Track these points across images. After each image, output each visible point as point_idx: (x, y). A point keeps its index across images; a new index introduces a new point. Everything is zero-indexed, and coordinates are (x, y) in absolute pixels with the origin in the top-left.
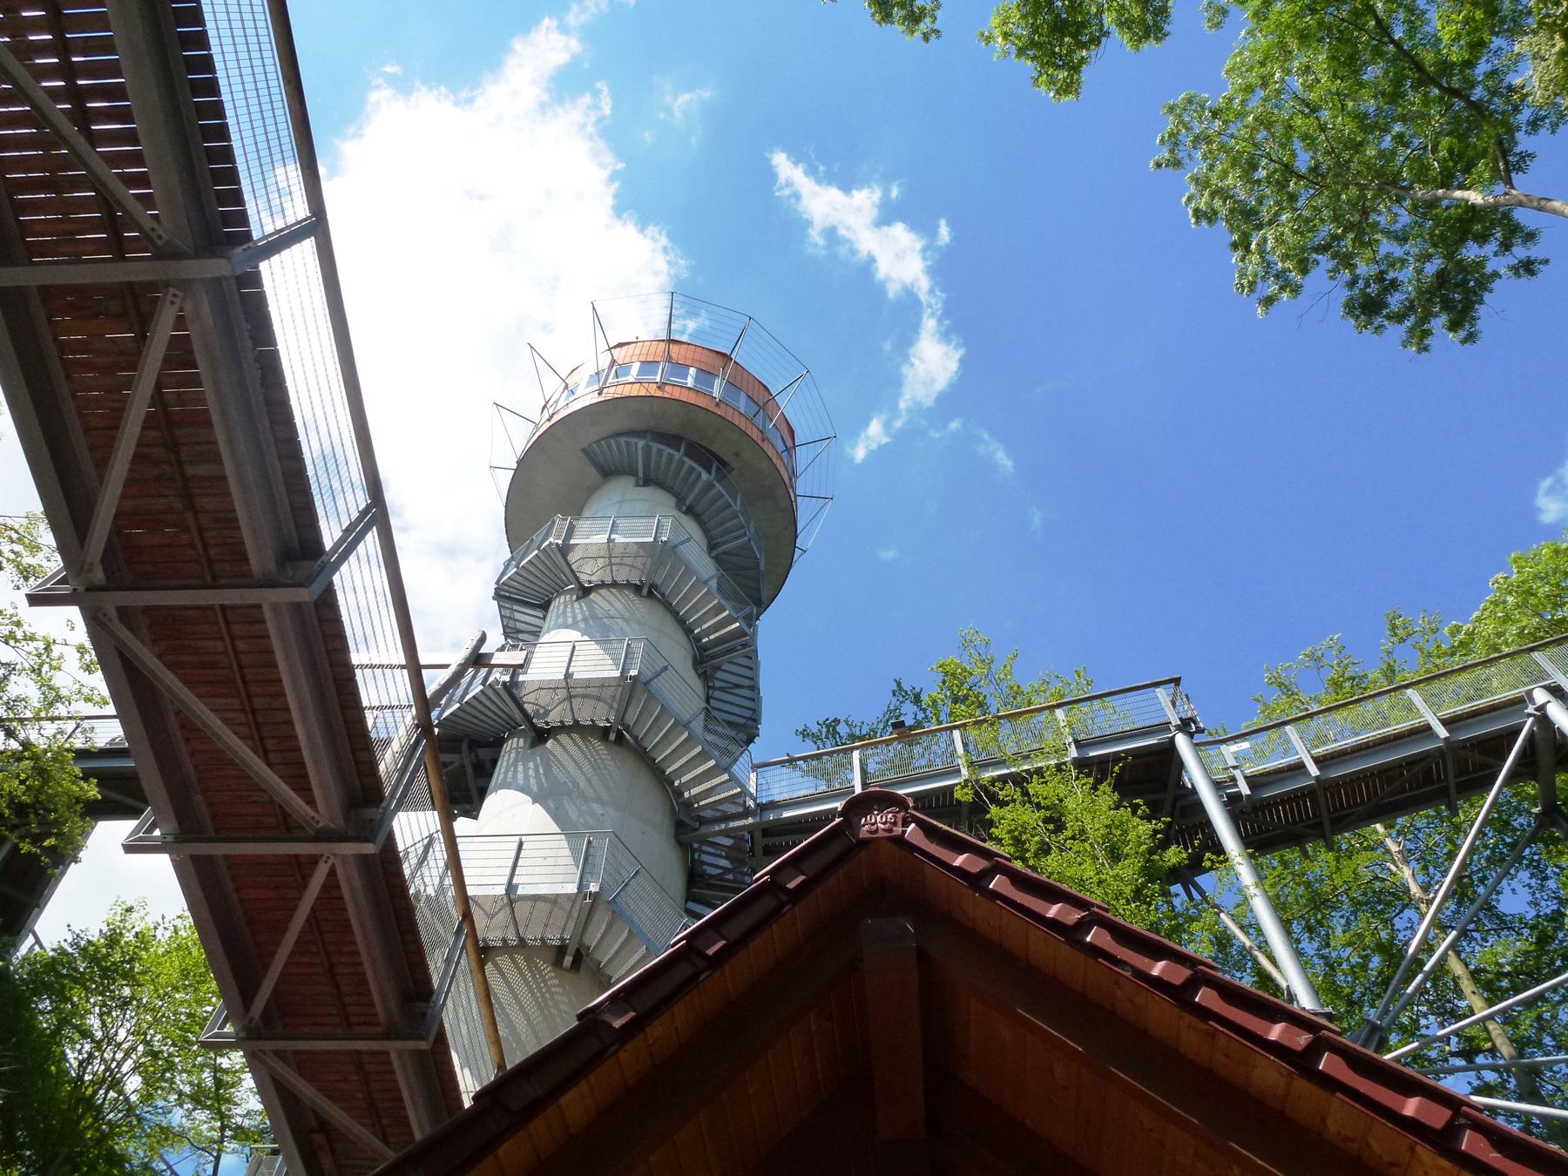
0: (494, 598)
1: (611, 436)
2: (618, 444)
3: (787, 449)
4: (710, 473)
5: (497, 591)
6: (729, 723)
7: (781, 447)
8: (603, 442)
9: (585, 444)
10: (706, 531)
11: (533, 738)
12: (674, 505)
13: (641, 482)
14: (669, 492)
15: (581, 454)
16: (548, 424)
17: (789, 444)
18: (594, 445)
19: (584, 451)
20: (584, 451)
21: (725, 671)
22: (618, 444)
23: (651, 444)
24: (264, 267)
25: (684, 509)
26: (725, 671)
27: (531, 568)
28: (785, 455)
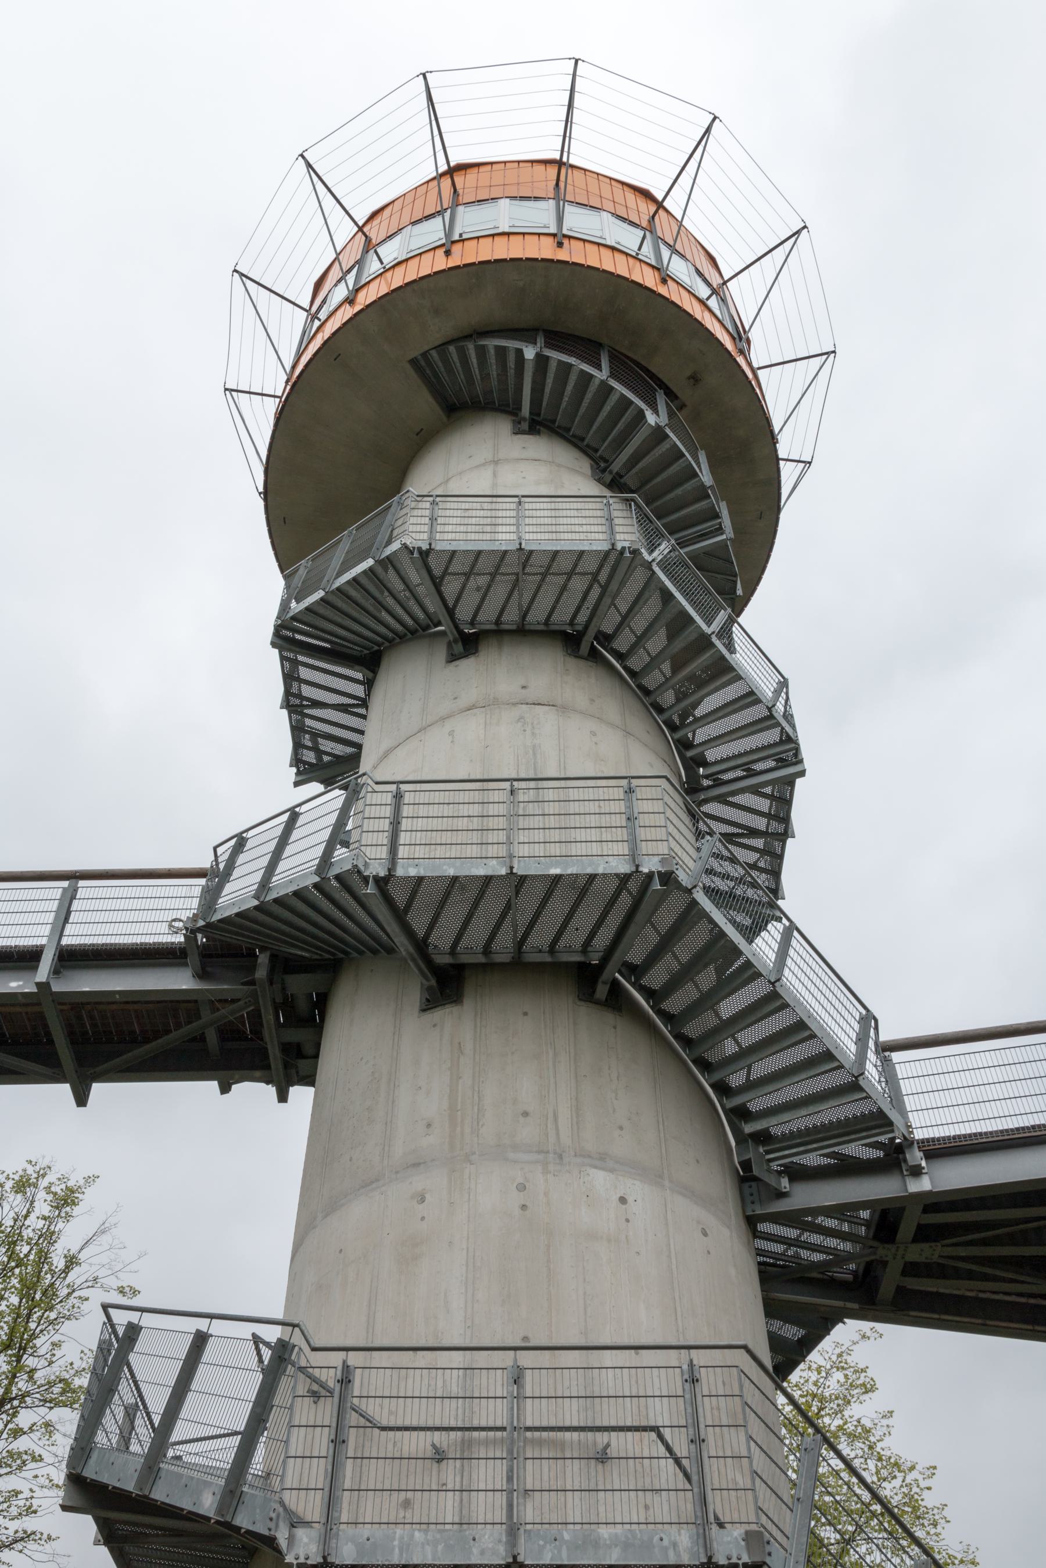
0: (274, 645)
1: (468, 337)
2: (482, 351)
3: (714, 292)
4: (656, 411)
5: (277, 633)
6: (1018, 1263)
7: (703, 292)
8: (452, 348)
9: (415, 353)
10: (588, 451)
11: (427, 946)
12: (589, 472)
13: (525, 426)
14: (576, 446)
15: (408, 366)
16: (348, 312)
17: (716, 281)
18: (434, 353)
19: (413, 362)
20: (413, 362)
21: (537, 574)
22: (482, 351)
23: (548, 352)
24: (66, 1088)
25: (608, 478)
26: (537, 574)
27: (339, 603)
28: (713, 303)
